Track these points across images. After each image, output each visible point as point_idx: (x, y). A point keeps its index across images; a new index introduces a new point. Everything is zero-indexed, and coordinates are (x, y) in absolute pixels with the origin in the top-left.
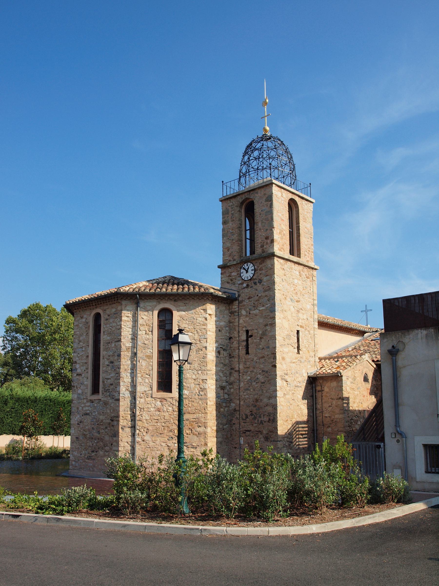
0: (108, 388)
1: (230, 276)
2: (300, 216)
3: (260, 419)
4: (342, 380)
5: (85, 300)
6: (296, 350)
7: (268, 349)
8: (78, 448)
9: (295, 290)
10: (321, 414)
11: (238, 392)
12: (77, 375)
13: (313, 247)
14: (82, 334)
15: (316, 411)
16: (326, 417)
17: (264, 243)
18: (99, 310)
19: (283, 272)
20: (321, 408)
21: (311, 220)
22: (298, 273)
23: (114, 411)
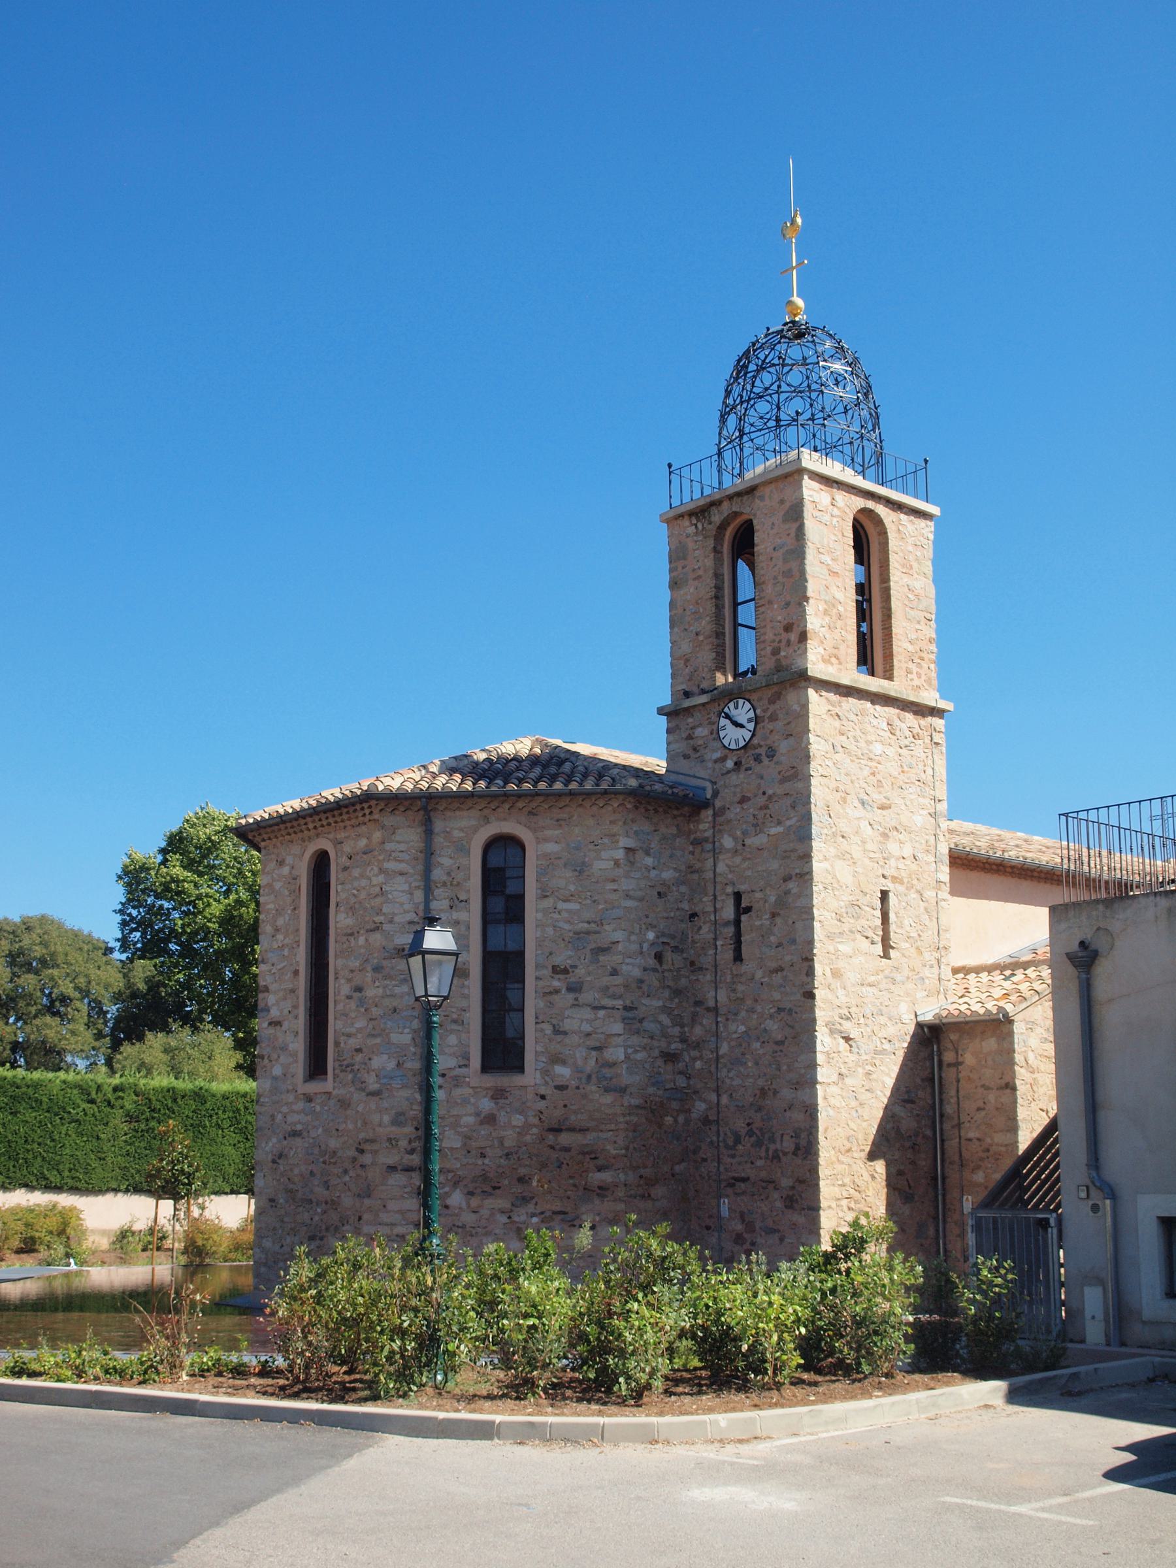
1: (690, 737)
2: (893, 559)
3: (772, 1147)
4: (1011, 1034)
5: (261, 821)
6: (878, 949)
7: (794, 947)
9: (873, 774)
10: (956, 1131)
11: (713, 1069)
12: (270, 1024)
13: (934, 648)
14: (283, 910)
15: (941, 1123)
16: (970, 1140)
17: (780, 641)
18: (324, 844)
19: (837, 723)
20: (956, 1117)
21: (928, 567)
22: (885, 726)
23: (365, 1123)
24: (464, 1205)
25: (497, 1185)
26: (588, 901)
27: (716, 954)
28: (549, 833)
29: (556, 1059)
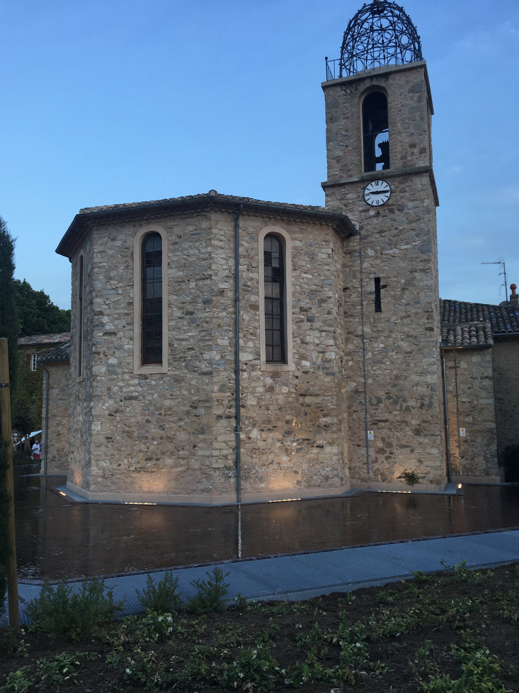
0: (182, 355)
1: (342, 199)
8: (112, 455)
11: (361, 365)
16: (464, 402)
20: (455, 391)
24: (259, 437)
25: (276, 425)
26: (316, 274)
27: (362, 308)
28: (297, 235)
29: (303, 357)
